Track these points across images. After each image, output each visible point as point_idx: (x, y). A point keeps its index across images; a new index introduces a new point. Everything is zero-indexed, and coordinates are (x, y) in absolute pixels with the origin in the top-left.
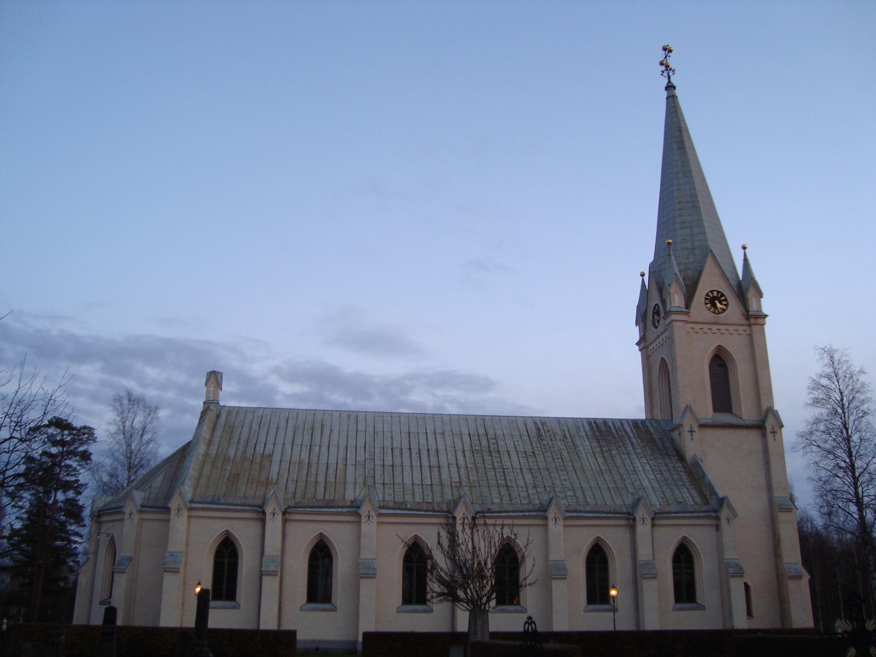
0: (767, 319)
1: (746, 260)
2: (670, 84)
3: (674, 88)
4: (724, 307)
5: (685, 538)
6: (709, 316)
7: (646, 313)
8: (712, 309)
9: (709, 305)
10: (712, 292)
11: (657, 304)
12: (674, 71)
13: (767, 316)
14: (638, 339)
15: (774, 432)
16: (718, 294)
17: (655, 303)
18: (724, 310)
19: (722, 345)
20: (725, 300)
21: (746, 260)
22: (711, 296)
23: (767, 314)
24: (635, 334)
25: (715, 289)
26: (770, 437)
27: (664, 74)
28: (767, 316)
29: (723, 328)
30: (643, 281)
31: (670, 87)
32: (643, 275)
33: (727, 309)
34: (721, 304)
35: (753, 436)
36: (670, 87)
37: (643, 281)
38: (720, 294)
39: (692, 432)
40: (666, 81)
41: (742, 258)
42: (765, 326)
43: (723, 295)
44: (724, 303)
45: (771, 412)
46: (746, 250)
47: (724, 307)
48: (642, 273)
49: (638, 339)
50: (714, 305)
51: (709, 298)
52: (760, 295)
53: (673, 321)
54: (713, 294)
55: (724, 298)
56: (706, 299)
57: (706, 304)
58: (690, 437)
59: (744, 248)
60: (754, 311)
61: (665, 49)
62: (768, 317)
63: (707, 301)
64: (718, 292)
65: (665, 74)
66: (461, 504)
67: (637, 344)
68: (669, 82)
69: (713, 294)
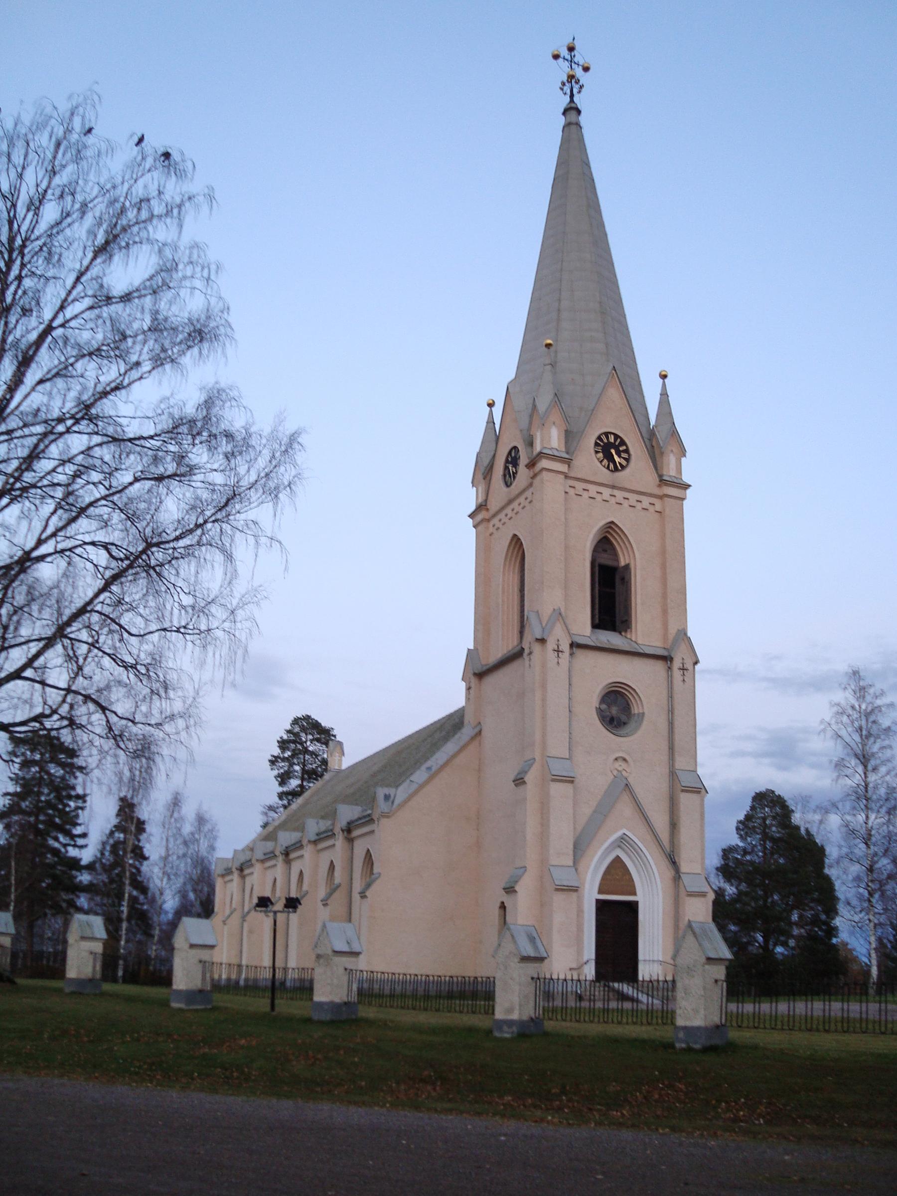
0: (689, 492)
1: (664, 395)
2: (573, 105)
3: (579, 112)
4: (624, 463)
5: (625, 836)
6: (602, 473)
7: (493, 464)
8: (605, 462)
9: (601, 455)
10: (607, 434)
11: (515, 448)
12: (581, 87)
13: (690, 486)
14: (513, 376)
15: (683, 669)
16: (616, 440)
17: (512, 445)
18: (623, 467)
19: (615, 521)
20: (627, 451)
21: (664, 395)
22: (605, 441)
23: (689, 483)
24: (470, 498)
25: (613, 431)
26: (677, 674)
27: (565, 88)
28: (690, 486)
29: (619, 494)
30: (491, 414)
31: (572, 110)
32: (491, 405)
33: (627, 465)
34: (620, 456)
35: (659, 666)
36: (572, 110)
37: (491, 414)
38: (619, 440)
39: (558, 651)
40: (567, 99)
41: (659, 390)
42: (685, 502)
43: (623, 443)
44: (624, 455)
45: (683, 635)
46: (666, 380)
47: (624, 463)
48: (491, 402)
49: (473, 507)
50: (610, 458)
51: (602, 444)
52: (683, 452)
53: (544, 469)
54: (607, 438)
55: (624, 448)
56: (596, 444)
57: (597, 452)
58: (556, 660)
59: (664, 377)
60: (670, 476)
61: (365, 897)
62: (691, 488)
63: (599, 449)
64: (617, 437)
65: (567, 89)
66: (874, 962)
67: (471, 516)
68: (572, 100)
69: (607, 438)
